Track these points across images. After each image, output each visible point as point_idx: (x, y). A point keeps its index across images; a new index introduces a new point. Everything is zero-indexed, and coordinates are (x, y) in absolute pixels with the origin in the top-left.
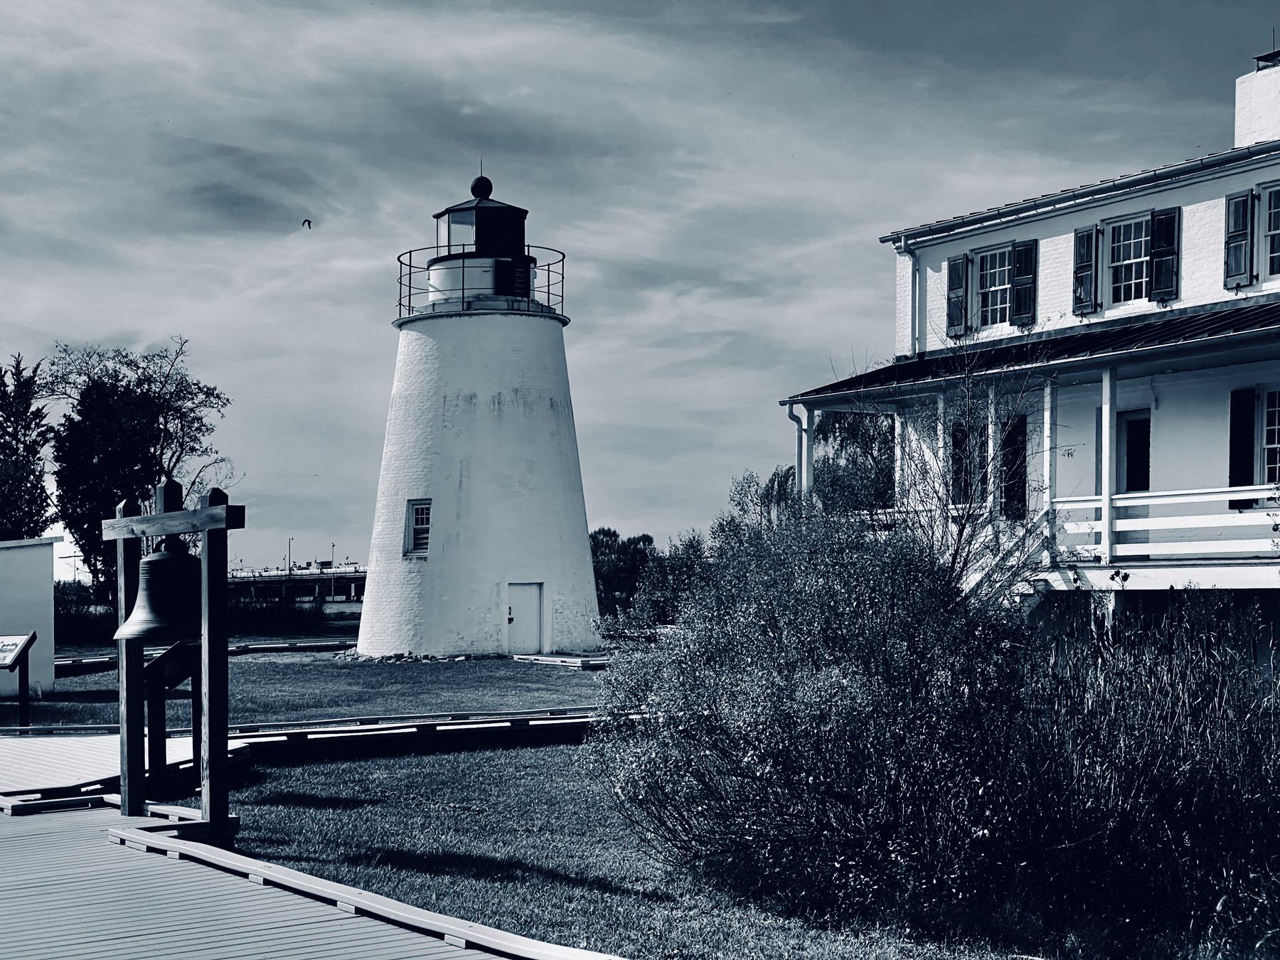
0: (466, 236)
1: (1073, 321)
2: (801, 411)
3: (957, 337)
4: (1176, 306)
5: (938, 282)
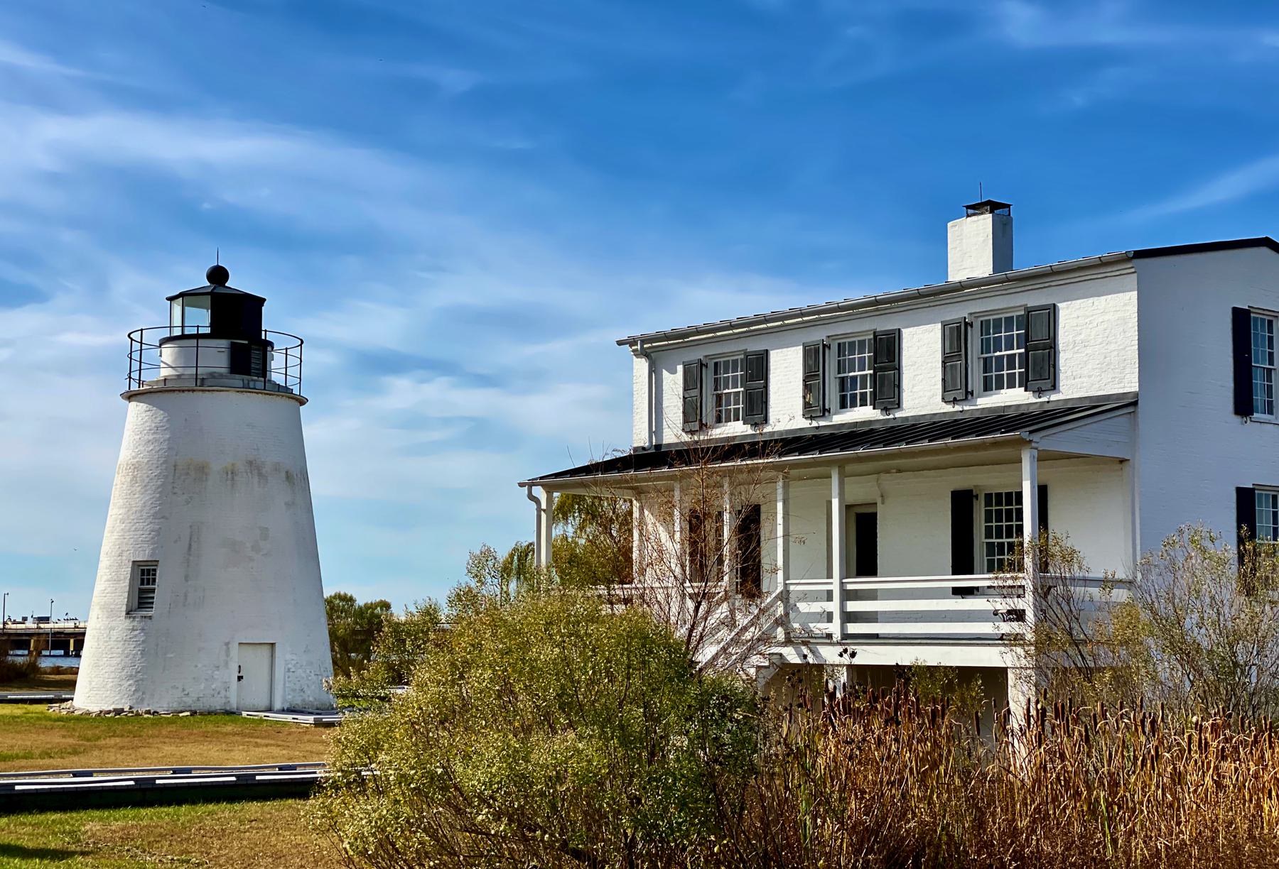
0: (201, 319)
2: (539, 492)
5: (673, 382)
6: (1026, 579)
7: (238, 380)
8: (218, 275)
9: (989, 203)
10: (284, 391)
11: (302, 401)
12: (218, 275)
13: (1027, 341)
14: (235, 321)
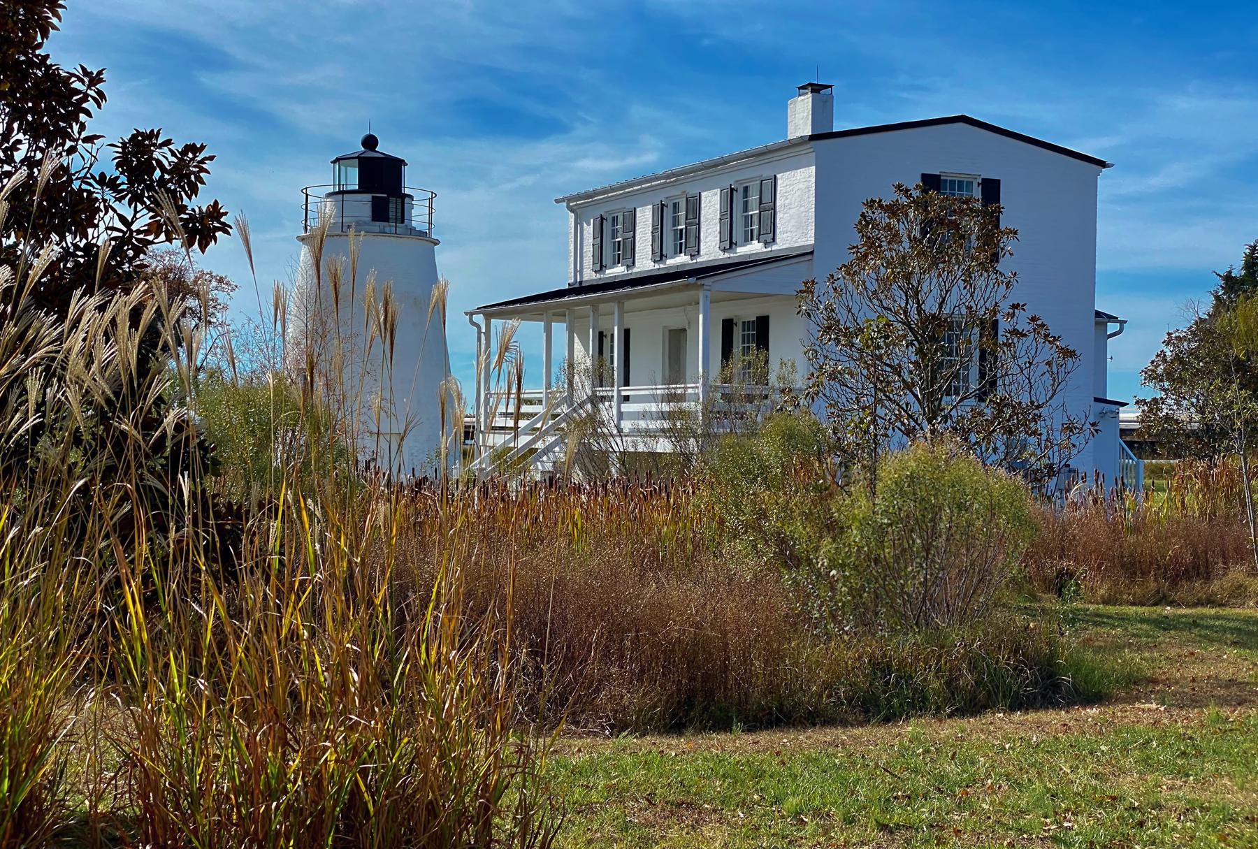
0: (352, 179)
1: (722, 255)
2: (479, 318)
3: (724, 250)
4: (775, 248)
5: (589, 230)
6: (700, 385)
7: (378, 225)
8: (370, 142)
9: (810, 84)
10: (422, 234)
11: (436, 243)
12: (370, 142)
13: (761, 203)
14: (380, 180)
